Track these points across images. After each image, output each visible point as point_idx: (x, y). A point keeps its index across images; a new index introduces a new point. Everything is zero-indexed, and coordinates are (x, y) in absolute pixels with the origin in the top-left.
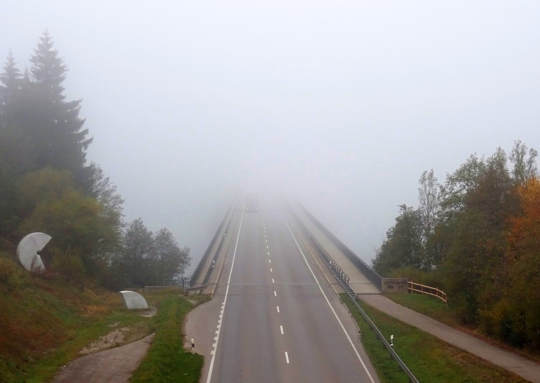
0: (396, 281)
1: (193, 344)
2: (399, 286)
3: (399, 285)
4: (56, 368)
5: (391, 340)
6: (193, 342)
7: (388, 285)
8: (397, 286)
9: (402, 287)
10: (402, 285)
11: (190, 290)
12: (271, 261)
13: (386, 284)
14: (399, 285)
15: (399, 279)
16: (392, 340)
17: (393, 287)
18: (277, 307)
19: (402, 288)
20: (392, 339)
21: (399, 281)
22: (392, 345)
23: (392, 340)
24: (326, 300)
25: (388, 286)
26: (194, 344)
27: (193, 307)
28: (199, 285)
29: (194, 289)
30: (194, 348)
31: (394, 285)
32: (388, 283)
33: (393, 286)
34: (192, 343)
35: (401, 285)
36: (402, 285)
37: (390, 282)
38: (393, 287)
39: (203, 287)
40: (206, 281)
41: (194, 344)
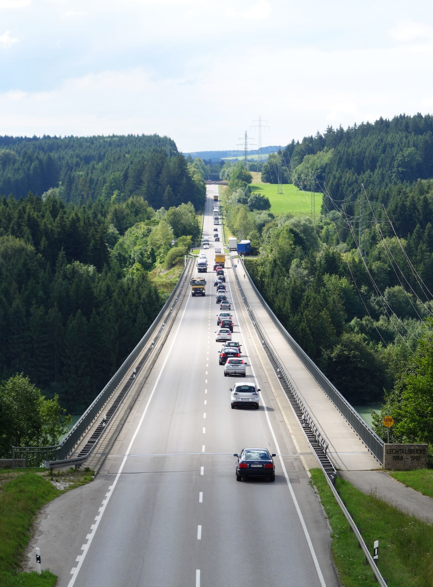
0: (407, 449)
1: (38, 556)
2: (412, 457)
3: (412, 455)
4: (168, 155)
5: (375, 549)
6: (39, 554)
7: (394, 455)
8: (409, 457)
9: (418, 458)
10: (418, 455)
11: (56, 466)
12: (206, 431)
13: (390, 453)
14: (412, 455)
15: (413, 446)
16: (376, 550)
17: (402, 459)
18: (202, 538)
19: (417, 460)
20: (377, 548)
21: (412, 448)
22: (376, 557)
23: (376, 550)
24: (325, 579)
25: (394, 457)
26: (40, 556)
27: (57, 494)
28: (75, 457)
29: (66, 462)
30: (40, 563)
31: (404, 455)
32: (394, 451)
33: (402, 457)
34: (37, 555)
35: (416, 455)
36: (418, 455)
37: (397, 450)
38: (402, 459)
39: (81, 460)
40: (86, 450)
41: (40, 556)
